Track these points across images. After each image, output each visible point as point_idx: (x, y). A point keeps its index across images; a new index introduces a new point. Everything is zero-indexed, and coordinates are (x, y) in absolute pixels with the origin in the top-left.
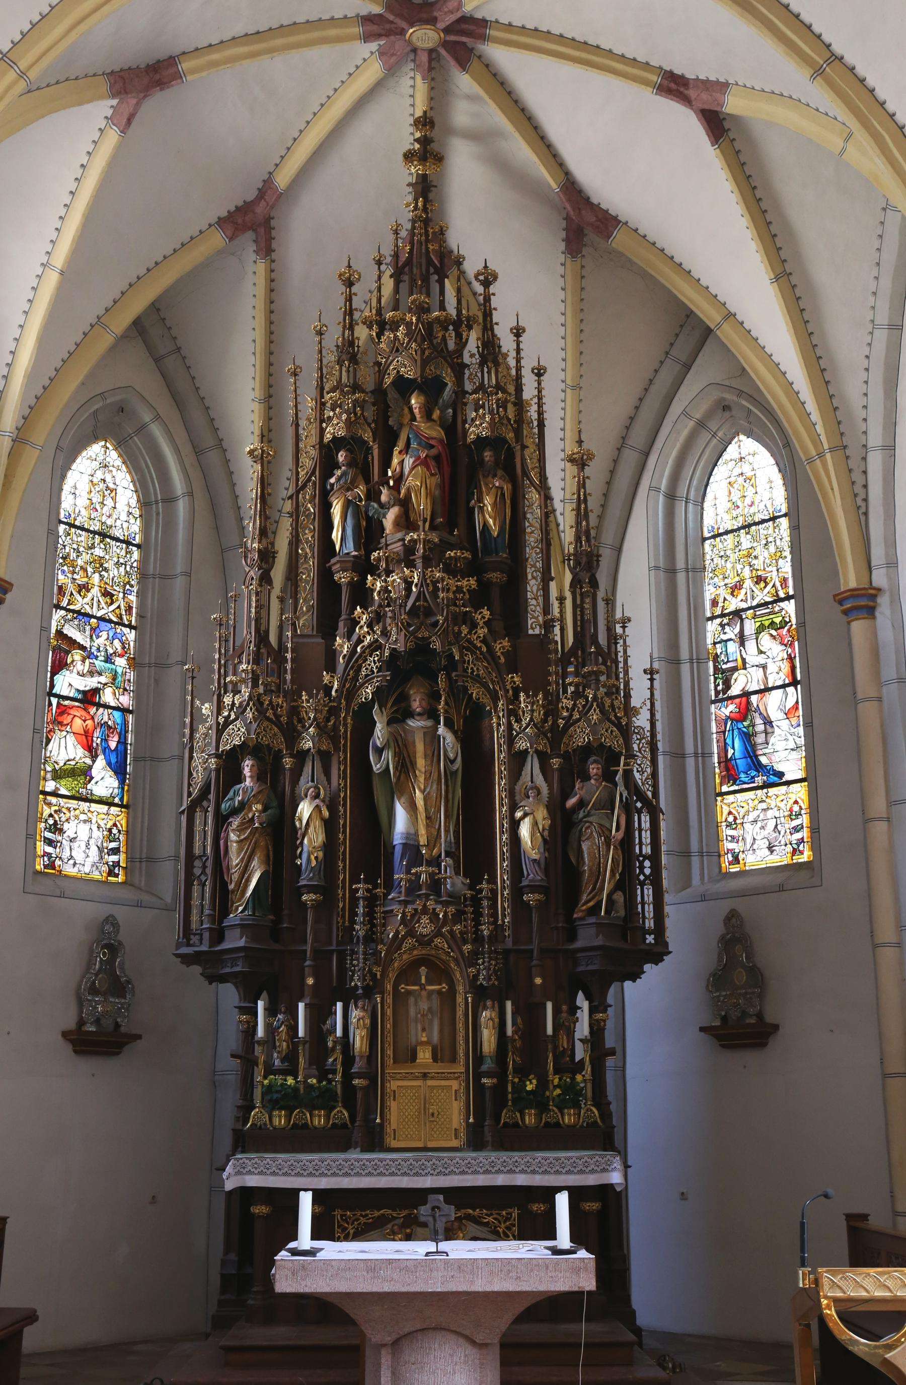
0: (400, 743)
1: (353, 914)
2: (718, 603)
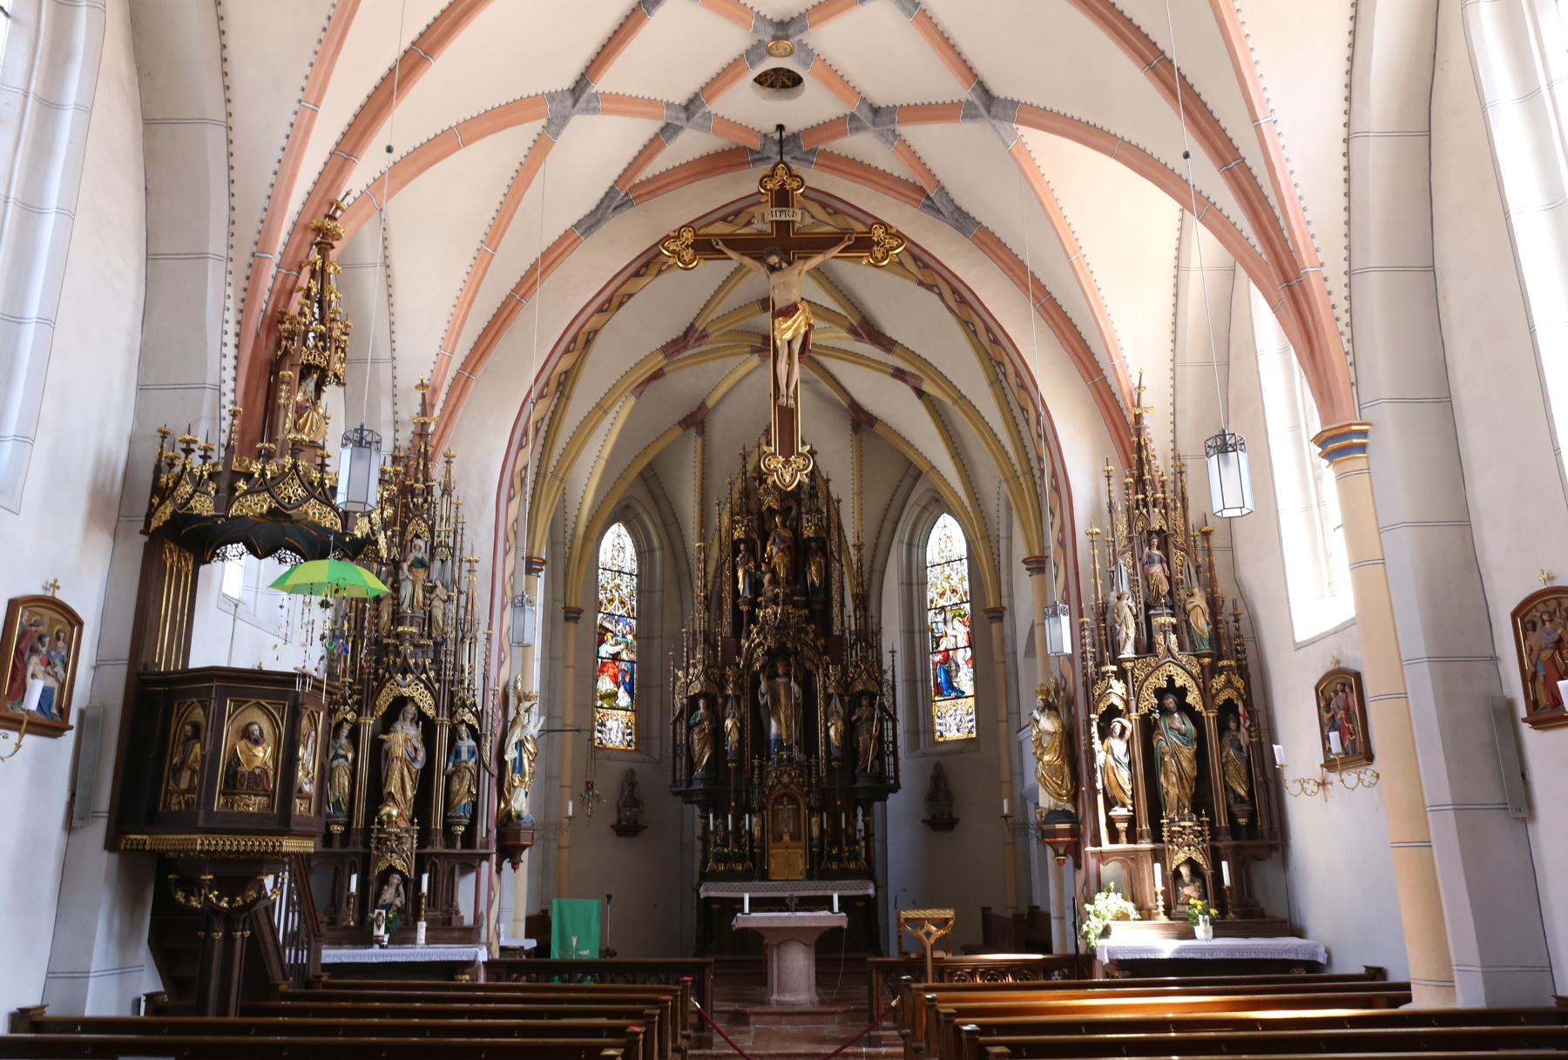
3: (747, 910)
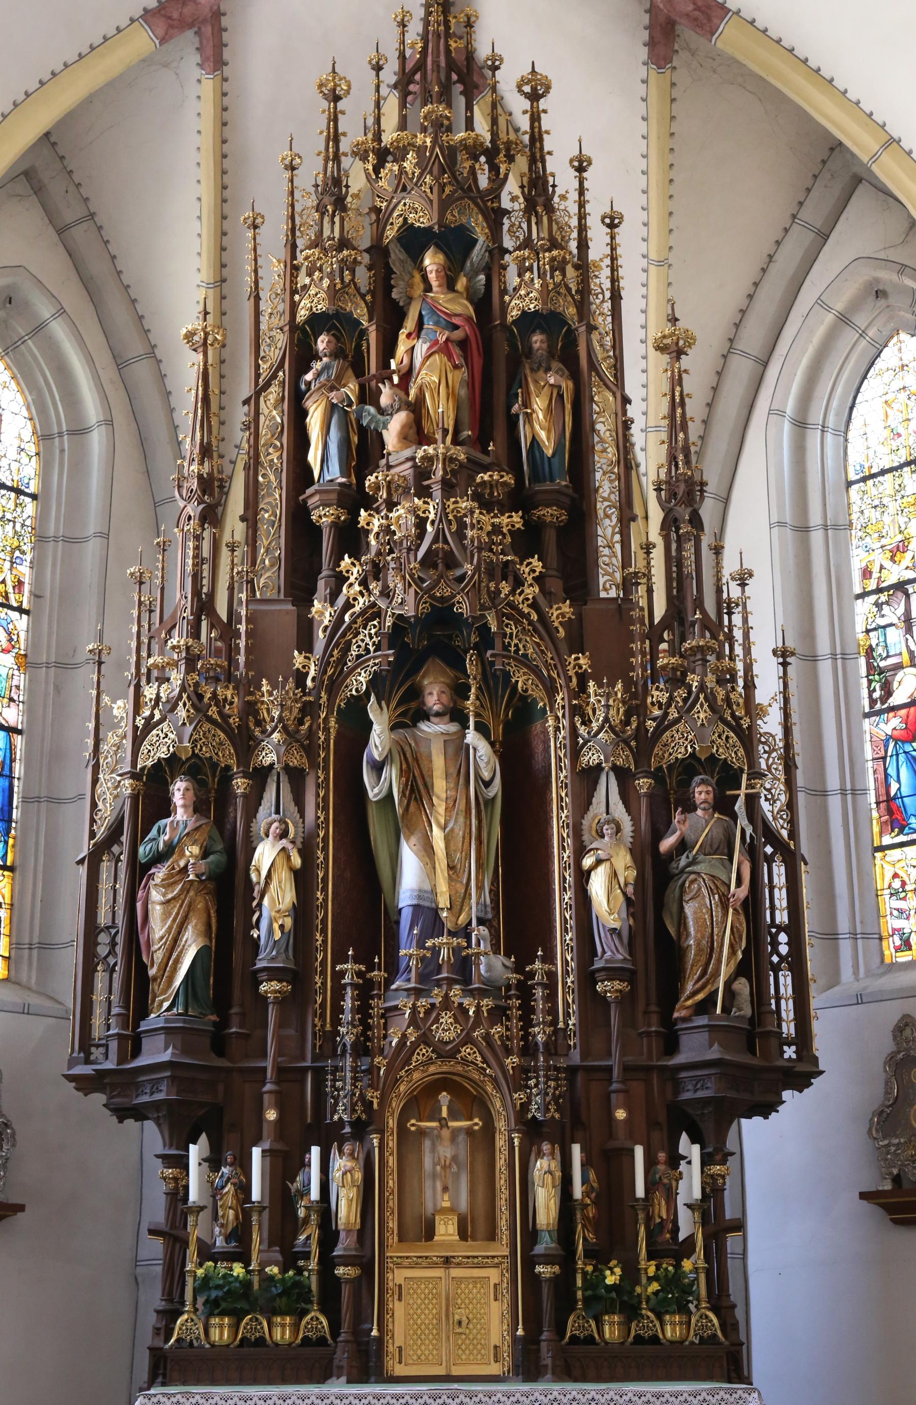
0: (409, 755)
1: (338, 1010)
2: (871, 573)
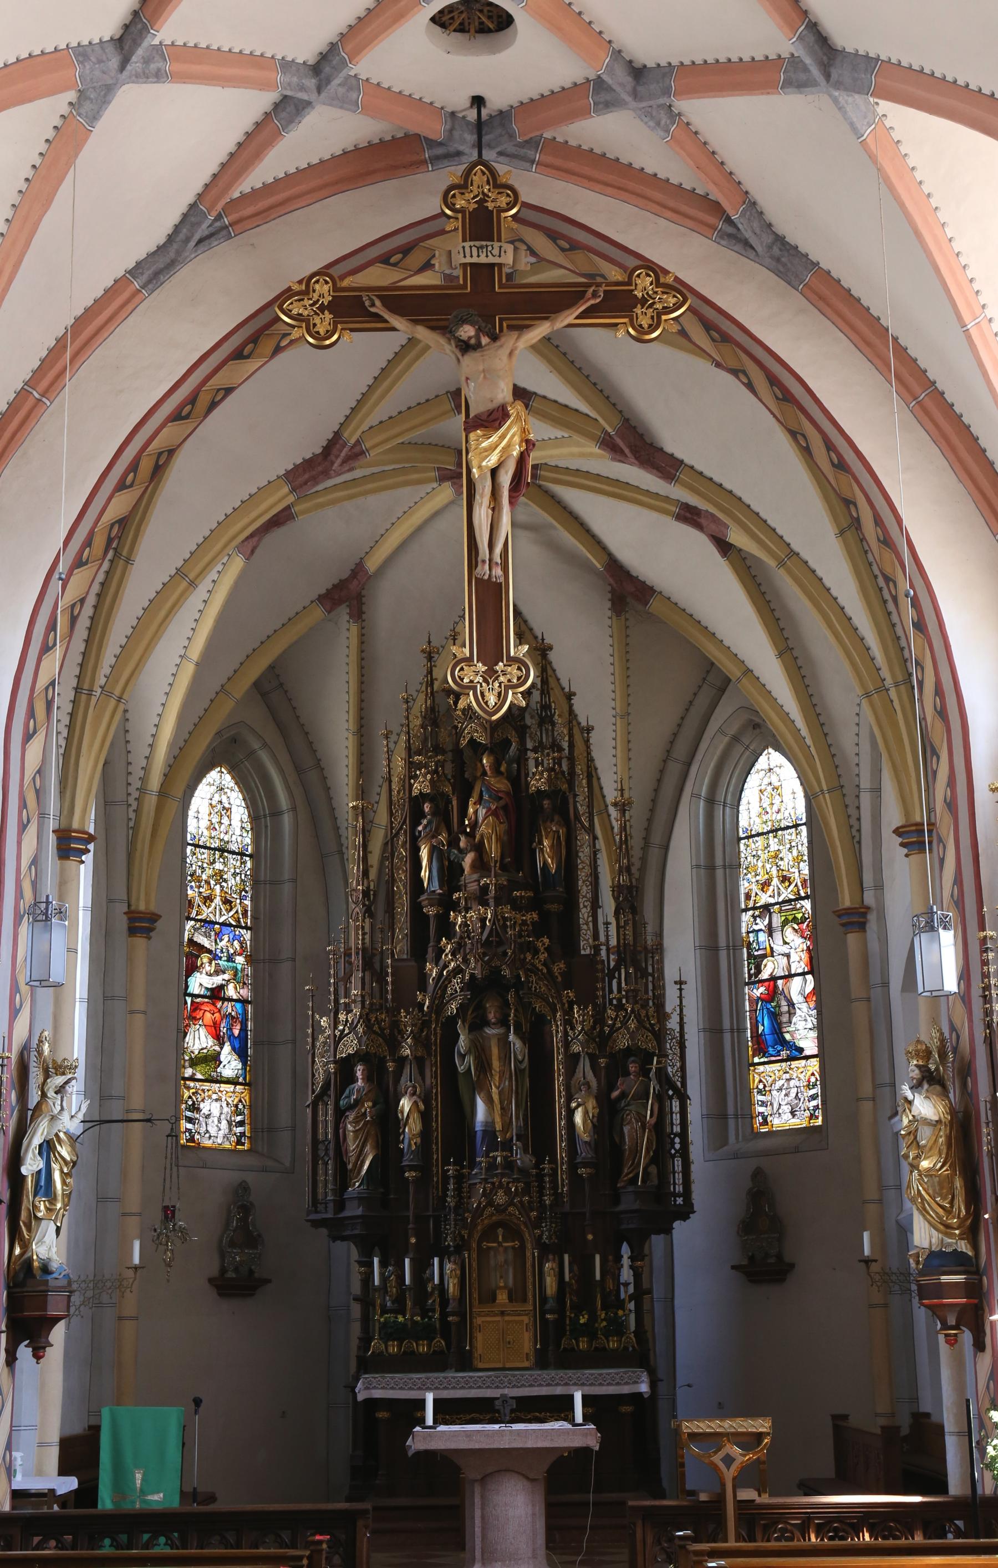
1: (445, 1189)
3: (430, 1420)
